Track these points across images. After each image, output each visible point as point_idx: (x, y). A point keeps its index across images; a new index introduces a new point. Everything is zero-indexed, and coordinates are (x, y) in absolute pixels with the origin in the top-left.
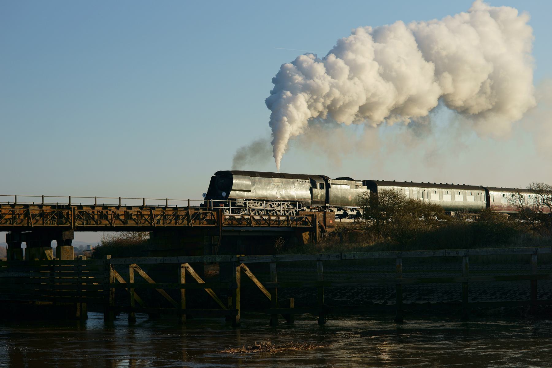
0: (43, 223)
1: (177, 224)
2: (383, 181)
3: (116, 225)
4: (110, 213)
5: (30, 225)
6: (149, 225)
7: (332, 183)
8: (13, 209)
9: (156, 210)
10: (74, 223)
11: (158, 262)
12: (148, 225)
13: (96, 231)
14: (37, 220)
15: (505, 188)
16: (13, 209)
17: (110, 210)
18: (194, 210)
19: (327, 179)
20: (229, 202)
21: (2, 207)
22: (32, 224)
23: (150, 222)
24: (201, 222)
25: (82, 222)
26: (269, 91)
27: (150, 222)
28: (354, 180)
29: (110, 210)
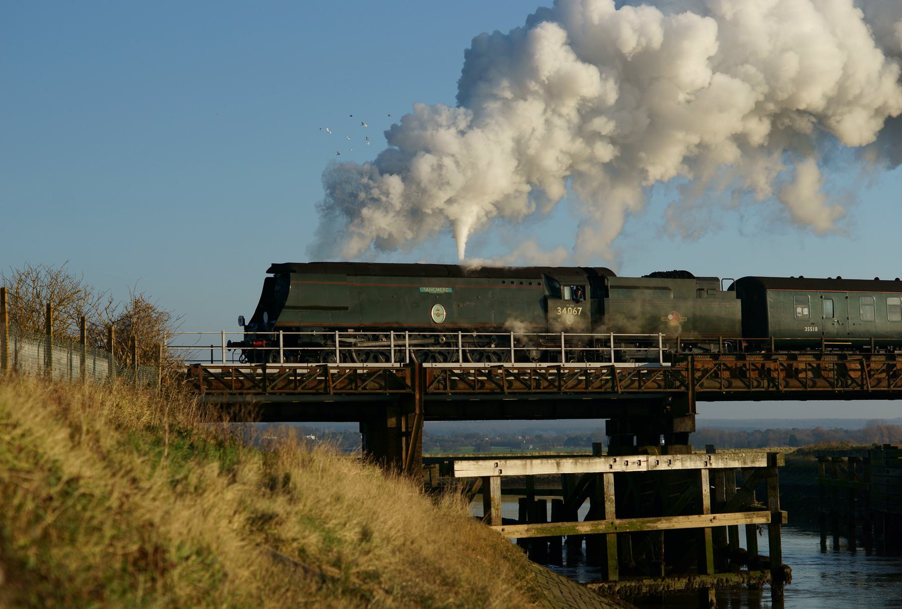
0: (889, 386)
1: (892, 387)
2: (801, 277)
3: (873, 389)
4: (832, 368)
5: (865, 388)
6: (858, 388)
7: (613, 284)
8: (891, 363)
9: (799, 359)
10: (694, 386)
11: (643, 468)
12: (856, 389)
13: (850, 400)
14: (879, 380)
15: (792, 277)
16: (891, 363)
17: (776, 362)
18: (884, 359)
19: (603, 275)
20: (278, 335)
21: (897, 359)
22: (869, 386)
23: (860, 383)
24: (891, 383)
25: (718, 382)
26: (463, 50)
27: (860, 383)
28: (695, 275)
29: (776, 362)
